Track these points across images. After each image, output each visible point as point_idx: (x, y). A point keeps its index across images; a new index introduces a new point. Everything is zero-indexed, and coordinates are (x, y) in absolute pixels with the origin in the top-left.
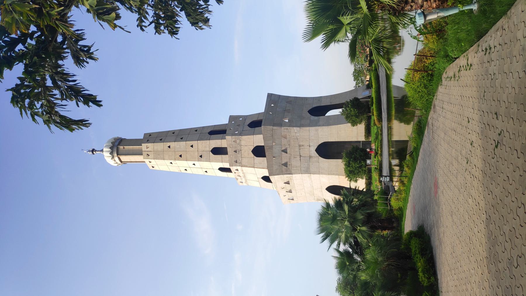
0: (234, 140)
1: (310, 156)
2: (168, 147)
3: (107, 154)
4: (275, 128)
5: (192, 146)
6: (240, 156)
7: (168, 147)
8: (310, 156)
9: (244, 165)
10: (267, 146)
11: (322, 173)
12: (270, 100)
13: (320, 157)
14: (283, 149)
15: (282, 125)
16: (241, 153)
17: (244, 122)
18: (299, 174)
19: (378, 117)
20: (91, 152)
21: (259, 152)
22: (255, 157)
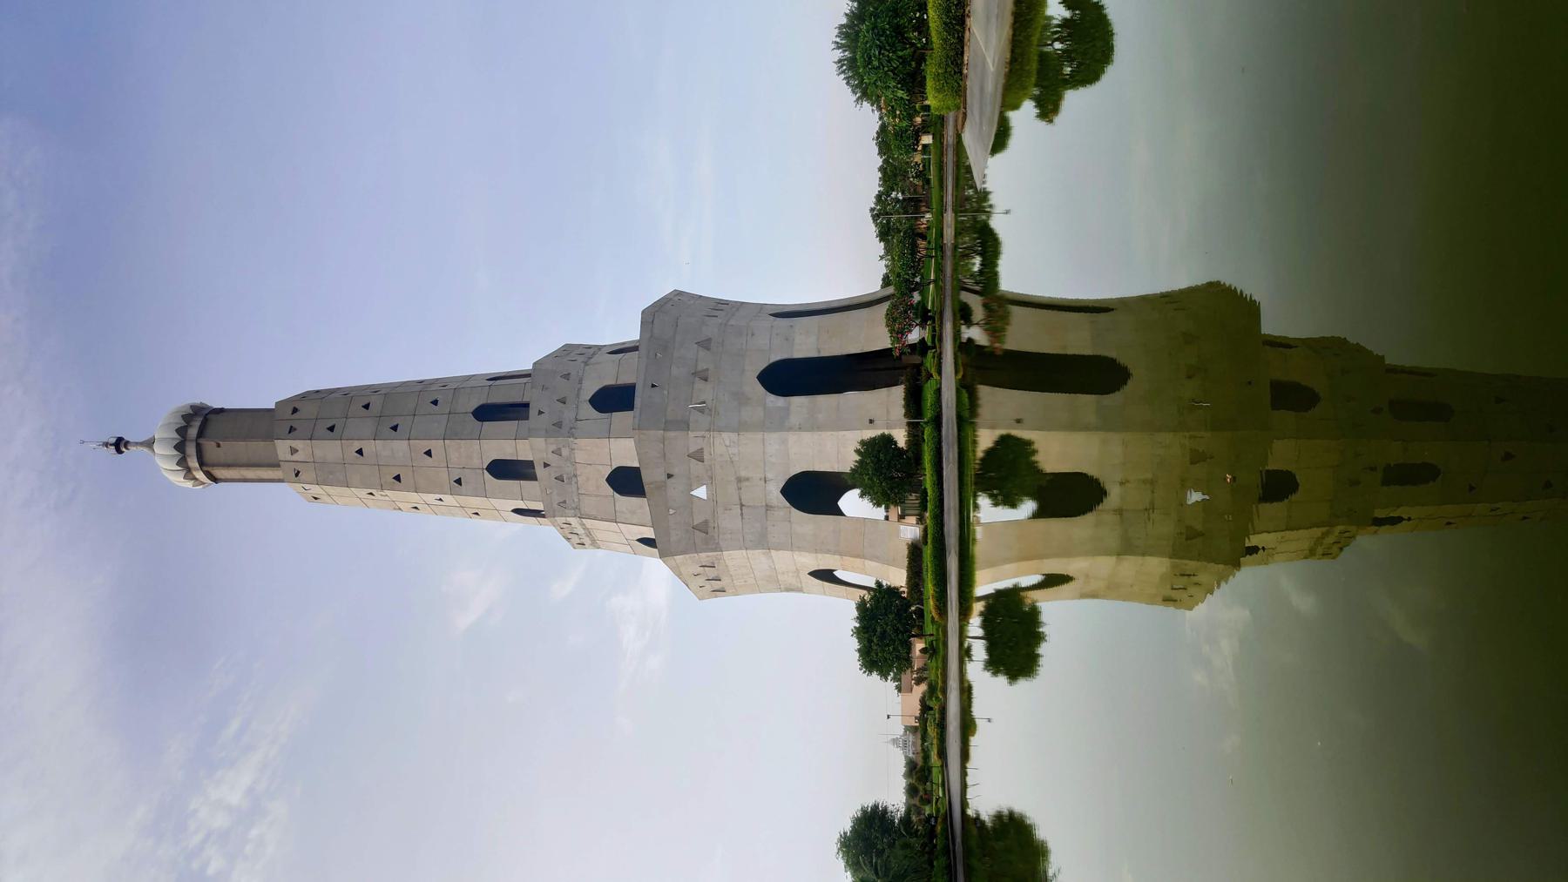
0: (554, 447)
1: (767, 505)
2: (357, 452)
3: (164, 461)
4: (672, 434)
5: (429, 453)
6: (574, 489)
7: (357, 452)
8: (767, 505)
9: (587, 515)
10: (651, 483)
11: (800, 549)
12: (651, 336)
13: (794, 510)
14: (692, 450)
15: (688, 428)
16: (577, 483)
17: (579, 389)
18: (741, 549)
19: (938, 603)
20: (113, 447)
21: (626, 481)
22: (617, 495)
